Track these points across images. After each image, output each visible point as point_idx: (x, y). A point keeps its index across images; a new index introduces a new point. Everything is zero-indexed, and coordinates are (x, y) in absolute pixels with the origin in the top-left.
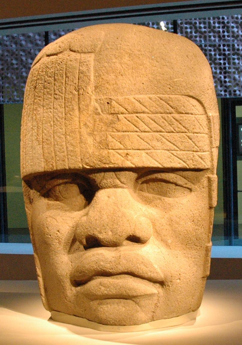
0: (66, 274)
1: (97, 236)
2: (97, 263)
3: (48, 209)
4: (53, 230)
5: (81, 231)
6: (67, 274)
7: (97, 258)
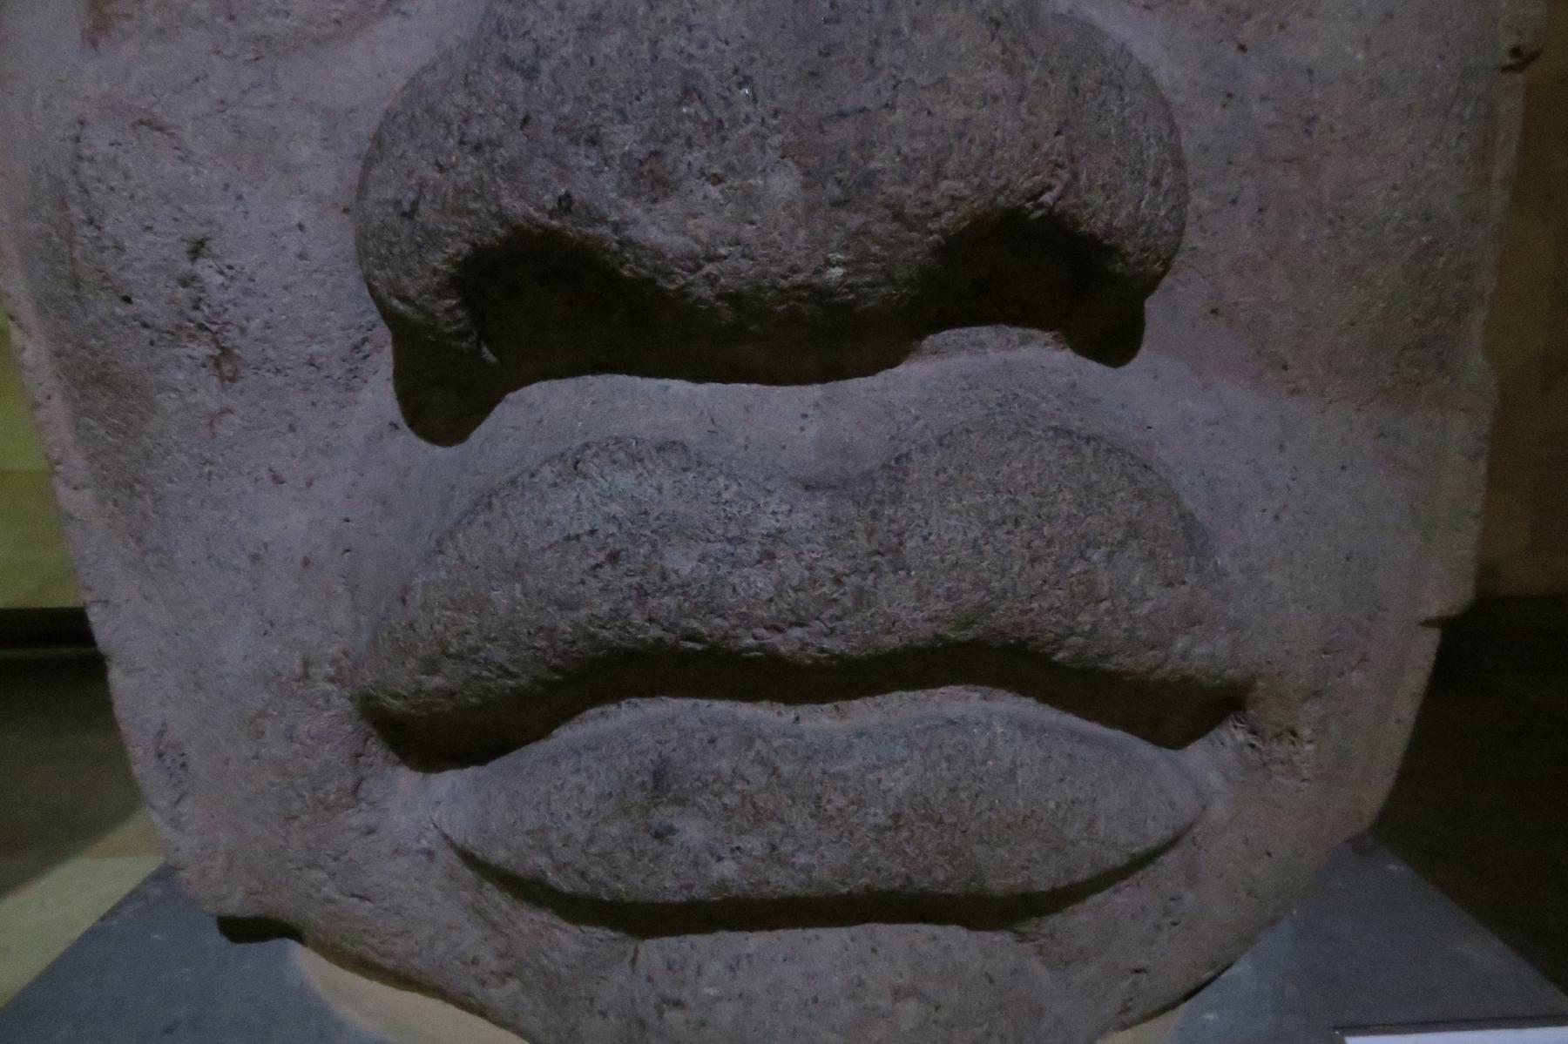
0: (299, 670)
1: (603, 230)
2: (614, 558)
3: (95, 44)
4: (149, 237)
5: (411, 196)
6: (306, 664)
7: (615, 508)
